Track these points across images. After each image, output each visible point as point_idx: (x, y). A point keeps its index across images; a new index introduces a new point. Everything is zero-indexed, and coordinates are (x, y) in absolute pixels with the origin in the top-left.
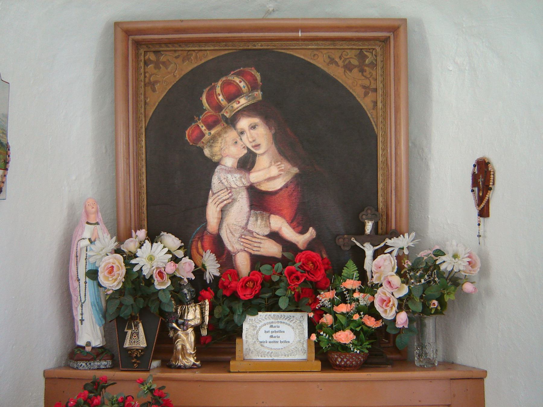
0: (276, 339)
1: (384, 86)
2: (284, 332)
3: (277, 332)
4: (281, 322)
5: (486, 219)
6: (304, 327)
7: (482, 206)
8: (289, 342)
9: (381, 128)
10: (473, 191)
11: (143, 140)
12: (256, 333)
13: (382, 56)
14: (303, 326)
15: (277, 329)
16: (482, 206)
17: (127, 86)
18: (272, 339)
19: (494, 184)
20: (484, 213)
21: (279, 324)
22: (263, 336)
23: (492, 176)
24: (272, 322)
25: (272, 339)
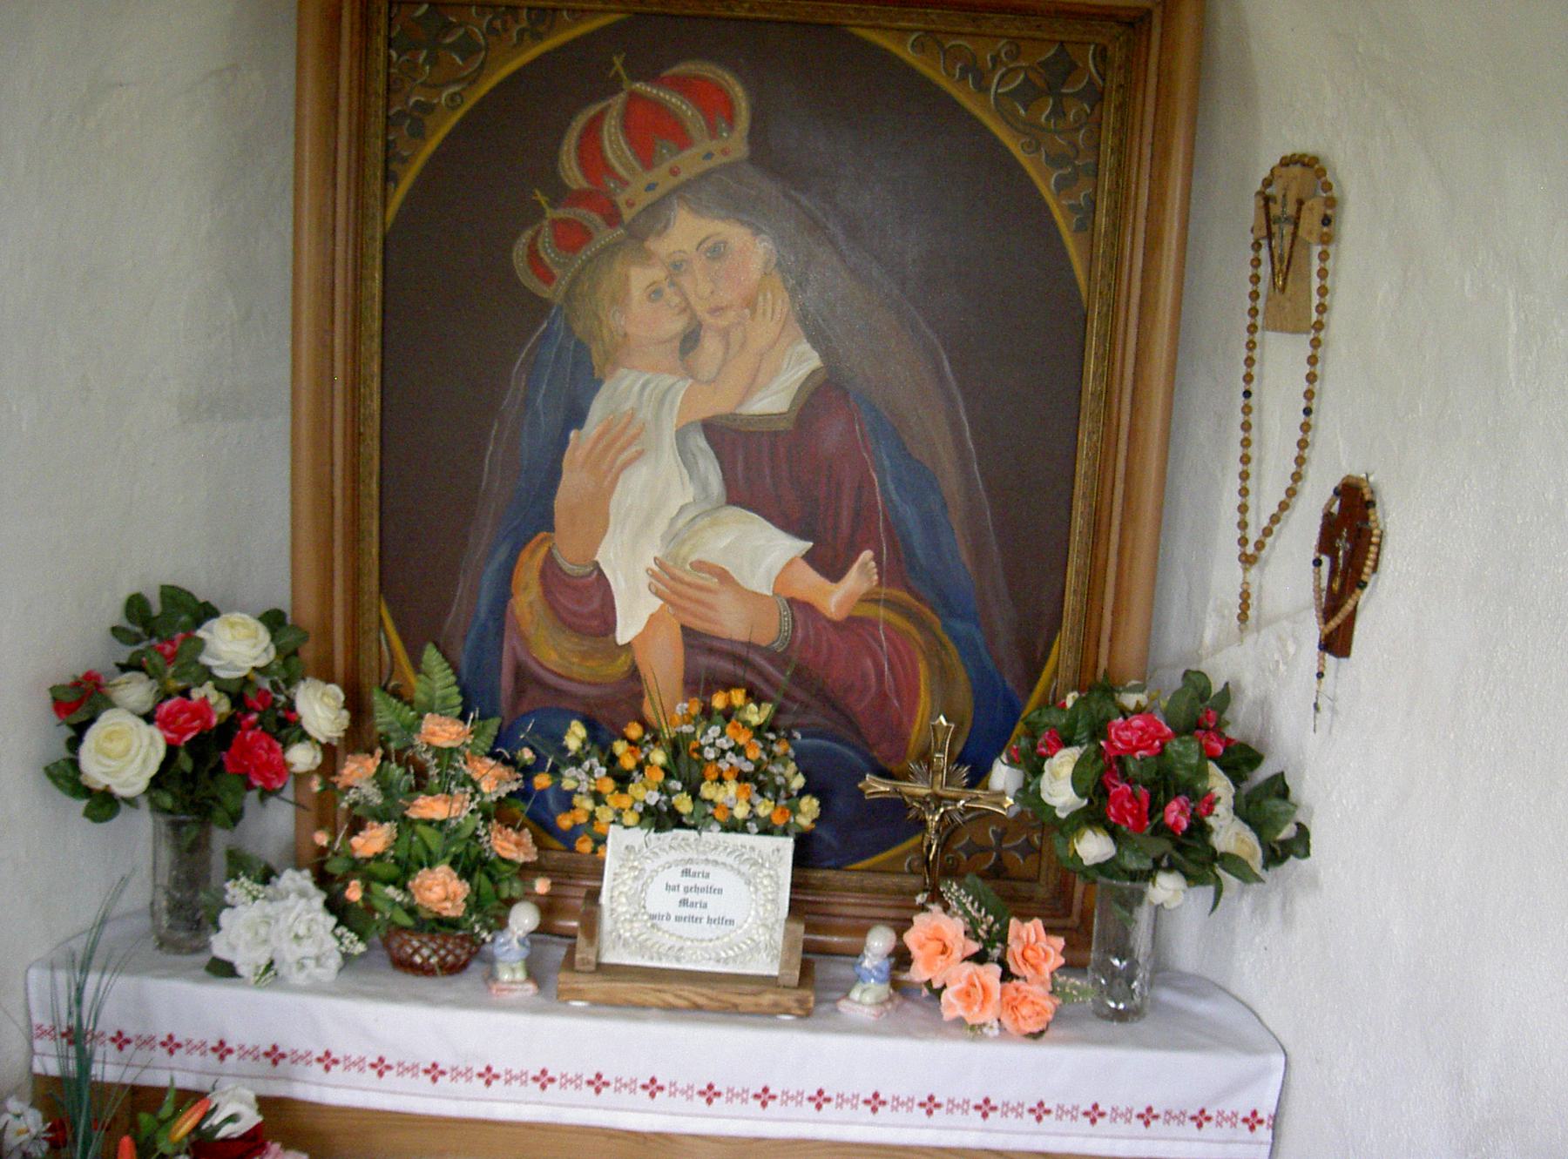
0: (696, 912)
1: (1120, 165)
2: (720, 891)
3: (702, 890)
4: (716, 863)
5: (1343, 660)
6: (781, 882)
7: (1333, 624)
8: (731, 922)
9: (1100, 293)
10: (1317, 563)
11: (377, 275)
12: (640, 888)
13: (1122, 71)
14: (778, 877)
15: (701, 882)
16: (1333, 624)
17: (335, 108)
18: (686, 911)
19: (1375, 569)
20: (1337, 643)
21: (708, 868)
22: (660, 901)
23: (1373, 549)
24: (690, 861)
25: (686, 911)
